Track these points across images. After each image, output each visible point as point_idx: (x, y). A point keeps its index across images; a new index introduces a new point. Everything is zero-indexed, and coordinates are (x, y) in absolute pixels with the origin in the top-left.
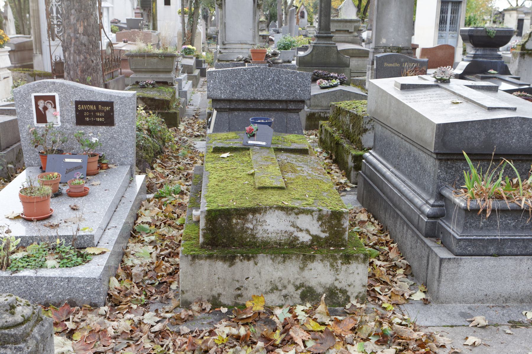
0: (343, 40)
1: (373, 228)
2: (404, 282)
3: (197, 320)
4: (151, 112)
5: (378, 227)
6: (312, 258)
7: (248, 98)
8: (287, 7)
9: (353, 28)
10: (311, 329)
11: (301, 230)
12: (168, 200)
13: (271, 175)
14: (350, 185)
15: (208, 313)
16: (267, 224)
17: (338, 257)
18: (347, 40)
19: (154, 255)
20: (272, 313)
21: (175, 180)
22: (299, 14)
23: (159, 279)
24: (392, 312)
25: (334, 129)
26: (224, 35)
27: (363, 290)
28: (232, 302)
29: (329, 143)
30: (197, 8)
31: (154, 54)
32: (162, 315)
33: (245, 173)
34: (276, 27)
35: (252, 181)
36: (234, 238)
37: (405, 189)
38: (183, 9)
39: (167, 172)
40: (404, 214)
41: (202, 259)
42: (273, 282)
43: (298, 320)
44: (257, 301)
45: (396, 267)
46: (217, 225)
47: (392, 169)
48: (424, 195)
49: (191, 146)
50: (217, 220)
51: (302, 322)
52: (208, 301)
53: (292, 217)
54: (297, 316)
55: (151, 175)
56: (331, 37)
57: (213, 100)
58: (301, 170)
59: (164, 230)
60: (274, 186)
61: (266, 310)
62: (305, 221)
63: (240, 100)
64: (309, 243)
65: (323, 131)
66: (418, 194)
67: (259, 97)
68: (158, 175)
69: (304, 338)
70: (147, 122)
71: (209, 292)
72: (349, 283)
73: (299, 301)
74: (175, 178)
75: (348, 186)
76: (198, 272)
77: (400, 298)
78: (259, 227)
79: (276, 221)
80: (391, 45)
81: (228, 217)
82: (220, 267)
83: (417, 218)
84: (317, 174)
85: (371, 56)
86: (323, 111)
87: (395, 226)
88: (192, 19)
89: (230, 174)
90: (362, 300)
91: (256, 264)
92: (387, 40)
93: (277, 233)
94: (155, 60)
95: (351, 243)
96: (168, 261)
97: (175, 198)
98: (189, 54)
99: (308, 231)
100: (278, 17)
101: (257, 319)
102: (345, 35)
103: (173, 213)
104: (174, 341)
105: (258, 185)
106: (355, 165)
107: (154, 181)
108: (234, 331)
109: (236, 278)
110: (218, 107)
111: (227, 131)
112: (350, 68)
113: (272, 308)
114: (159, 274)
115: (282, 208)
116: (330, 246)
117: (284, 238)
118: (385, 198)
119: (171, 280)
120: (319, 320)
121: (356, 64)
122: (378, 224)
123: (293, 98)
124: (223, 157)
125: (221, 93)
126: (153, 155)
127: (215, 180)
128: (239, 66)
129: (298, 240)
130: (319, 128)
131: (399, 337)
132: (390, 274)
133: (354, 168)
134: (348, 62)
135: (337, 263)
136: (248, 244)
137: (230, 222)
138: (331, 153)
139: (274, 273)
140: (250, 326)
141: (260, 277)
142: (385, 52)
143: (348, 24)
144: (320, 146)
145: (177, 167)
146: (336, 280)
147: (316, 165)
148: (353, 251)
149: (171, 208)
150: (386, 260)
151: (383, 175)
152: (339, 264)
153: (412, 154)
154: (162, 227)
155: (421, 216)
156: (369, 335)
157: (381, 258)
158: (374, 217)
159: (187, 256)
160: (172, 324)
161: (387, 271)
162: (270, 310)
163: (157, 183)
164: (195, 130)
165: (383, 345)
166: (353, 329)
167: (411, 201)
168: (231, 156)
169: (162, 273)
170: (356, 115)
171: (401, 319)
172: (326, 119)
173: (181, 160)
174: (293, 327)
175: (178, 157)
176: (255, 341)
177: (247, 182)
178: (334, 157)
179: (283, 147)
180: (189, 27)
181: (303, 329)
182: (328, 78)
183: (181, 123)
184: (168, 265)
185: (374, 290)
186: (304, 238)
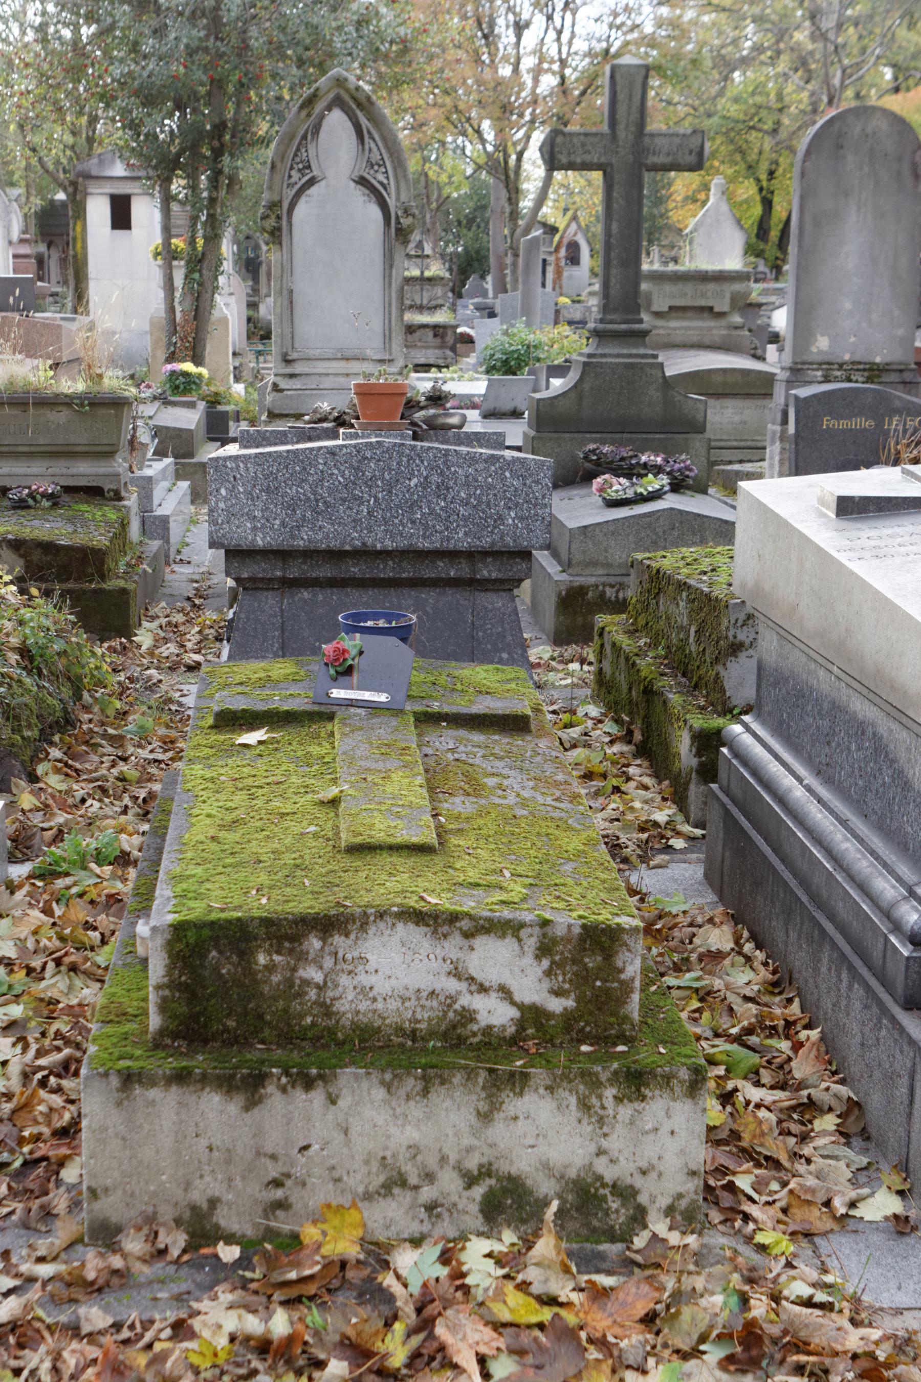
0: (695, 339)
2: (836, 1158)
3: (140, 1286)
4: (34, 591)
5: (765, 974)
6: (518, 1082)
7: (344, 544)
8: (518, 231)
9: (727, 300)
10: (506, 1316)
11: (483, 989)
12: (75, 884)
13: (395, 803)
14: (687, 829)
15: (177, 1262)
16: (371, 967)
17: (604, 1077)
18: (706, 341)
19: (14, 1069)
20: (387, 1263)
21: (106, 817)
22: (563, 252)
23: (26, 1149)
24: (783, 1261)
25: (642, 642)
26: (287, 331)
27: (691, 1187)
28: (256, 1225)
29: (625, 688)
30: (213, 239)
31: (57, 396)
32: (24, 1268)
33: (309, 797)
34: (484, 294)
35: (329, 825)
36: (260, 1016)
37: (845, 845)
38: (167, 243)
39: (80, 789)
40: (842, 929)
41: (154, 1084)
42: (389, 1160)
43: (466, 1290)
44: (336, 1222)
45: (811, 1108)
46: (207, 973)
47: (809, 779)
48: (904, 870)
49: (170, 700)
50: (203, 957)
51: (480, 1295)
52: (178, 1222)
53: (453, 947)
54: (463, 1275)
55: (27, 800)
56: (644, 334)
57: (228, 552)
58: (500, 787)
59: (54, 985)
61: (369, 1253)
62: (494, 959)
63: (317, 552)
64: (511, 1030)
65: (608, 648)
66: (885, 865)
67: (381, 540)
68: (50, 802)
69: (483, 1349)
70: (21, 623)
71: (178, 1194)
72: (644, 1164)
73: (478, 1222)
74: (108, 811)
75: (679, 834)
76: (140, 1126)
77: (818, 1213)
78: (344, 980)
79: (398, 959)
80: (847, 357)
81: (243, 946)
83: (880, 946)
84: (549, 801)
85: (779, 392)
86: (611, 580)
87: (816, 970)
88: (196, 276)
89: (259, 803)
90: (685, 1217)
91: (333, 1102)
92: (833, 339)
93: (404, 1000)
94: (61, 416)
95: (653, 1029)
96: (58, 1090)
97: (104, 879)
98: (186, 391)
99: (505, 992)
100: (492, 260)
101: (336, 1283)
102: (700, 324)
103: (88, 926)
104: (57, 1357)
105: (346, 838)
106: (701, 764)
107: (37, 819)
108: (253, 1325)
109: (269, 1148)
110: (245, 575)
111: (276, 655)
112: (709, 434)
113: (388, 1248)
114: (26, 1134)
115: (418, 917)
116: (581, 1042)
117: (426, 1015)
118: (787, 875)
119: (64, 1151)
120: (536, 1289)
121: (737, 419)
122: (765, 964)
123: (493, 543)
124: (245, 746)
125: (254, 529)
127: (208, 821)
128: (318, 438)
129: (472, 1020)
130: (596, 637)
131: (801, 1346)
132: (789, 1133)
133: (698, 772)
134: (700, 417)
135: (600, 1097)
136: (309, 1035)
137: (249, 963)
138: (631, 723)
139: (393, 1130)
140: (309, 1308)
141: (348, 1143)
142: (827, 380)
143: (711, 286)
144: (596, 698)
145: (115, 771)
146: (600, 1152)
147: (549, 768)
148: (655, 1058)
149: (80, 912)
150: (781, 1086)
151: (782, 800)
152: (609, 1102)
153: (869, 733)
154: (48, 974)
155: (892, 938)
156: (703, 1339)
157: (766, 1077)
158: (753, 937)
159: (106, 1075)
160: (56, 1301)
161: (780, 1122)
162: (378, 1255)
163: (45, 825)
164: (189, 645)
165: (744, 1372)
166: (649, 1319)
167: (863, 888)
168: (273, 741)
169: (35, 1130)
170: (708, 596)
171: (814, 1285)
172: (619, 607)
173: (130, 750)
174: (449, 1312)
175: (121, 738)
176: (322, 1356)
177: (312, 829)
178: (638, 737)
179: (447, 709)
180: (188, 303)
181: (482, 1317)
182: (631, 471)
183: (145, 624)
184: (57, 1100)
185: (731, 1187)
186: (495, 1014)
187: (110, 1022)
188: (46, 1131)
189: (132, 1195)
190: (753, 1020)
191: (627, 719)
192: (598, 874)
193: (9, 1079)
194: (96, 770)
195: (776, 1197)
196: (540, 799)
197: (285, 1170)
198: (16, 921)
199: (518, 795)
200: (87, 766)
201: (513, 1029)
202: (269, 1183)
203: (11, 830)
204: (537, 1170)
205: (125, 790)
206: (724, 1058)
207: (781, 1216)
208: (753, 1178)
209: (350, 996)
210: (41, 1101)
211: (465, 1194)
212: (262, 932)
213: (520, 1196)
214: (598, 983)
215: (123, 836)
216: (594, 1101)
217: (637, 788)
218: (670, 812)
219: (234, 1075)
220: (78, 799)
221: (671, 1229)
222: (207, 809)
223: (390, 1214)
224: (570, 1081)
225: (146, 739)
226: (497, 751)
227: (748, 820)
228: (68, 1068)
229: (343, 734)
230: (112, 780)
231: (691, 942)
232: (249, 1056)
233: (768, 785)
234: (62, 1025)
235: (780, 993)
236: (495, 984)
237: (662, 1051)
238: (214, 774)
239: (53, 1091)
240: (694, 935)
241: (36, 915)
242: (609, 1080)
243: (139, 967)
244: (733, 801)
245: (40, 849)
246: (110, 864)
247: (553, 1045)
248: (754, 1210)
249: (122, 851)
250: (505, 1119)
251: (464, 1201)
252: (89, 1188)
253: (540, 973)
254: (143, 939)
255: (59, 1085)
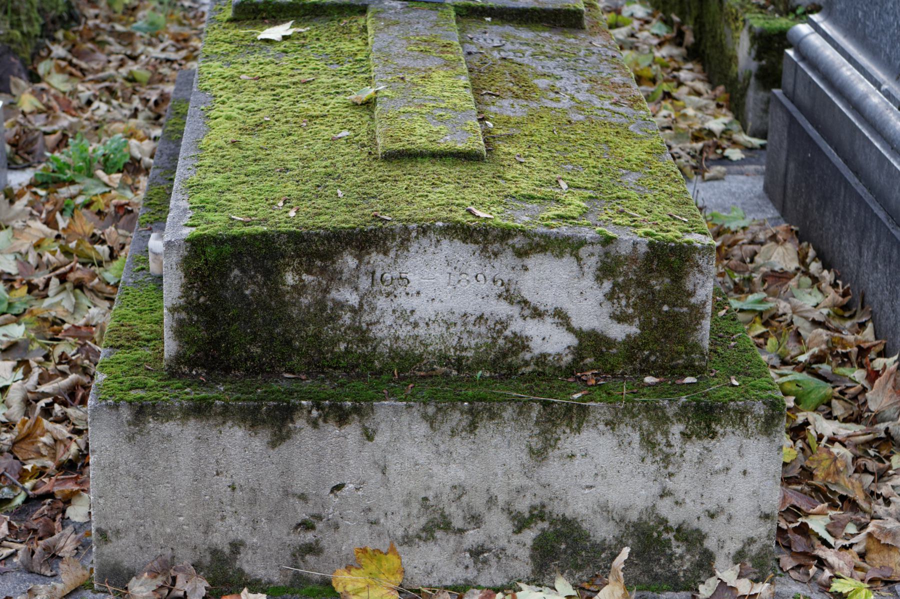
1: (818, 298)
5: (833, 296)
6: (576, 416)
11: (537, 314)
12: (80, 193)
14: (743, 138)
16: (413, 287)
17: (670, 411)
19: (15, 396)
21: (114, 120)
23: (28, 485)
27: (763, 531)
33: (341, 98)
35: (364, 129)
36: (288, 343)
39: (85, 91)
41: (169, 417)
42: (432, 502)
44: (372, 568)
46: (228, 295)
50: (224, 275)
53: (503, 266)
55: (28, 102)
58: (552, 89)
59: (57, 302)
60: (442, 147)
64: (568, 359)
68: (54, 103)
71: (198, 537)
72: (713, 508)
75: (735, 144)
78: (382, 303)
79: (443, 280)
82: (238, 447)
84: (607, 104)
89: (285, 104)
91: (370, 438)
93: (449, 325)
95: (723, 359)
96: (64, 419)
97: (111, 187)
99: (562, 317)
103: (96, 240)
105: (383, 144)
107: (39, 123)
114: (28, 467)
116: (645, 372)
117: (473, 342)
118: (861, 189)
119: (71, 487)
122: (835, 285)
124: (268, 41)
126: (37, 29)
127: (228, 124)
129: (525, 348)
132: (866, 471)
133: (757, 77)
135: (666, 433)
136: (343, 363)
138: (682, 23)
139: (436, 469)
141: (386, 483)
145: (124, 71)
146: (665, 494)
147: (606, 69)
148: (728, 391)
149: (86, 224)
150: (855, 419)
151: (857, 107)
154: (52, 290)
157: (839, 409)
158: (820, 256)
159: (116, 406)
161: (855, 458)
163: (48, 129)
169: (38, 463)
177: (345, 133)
178: (689, 38)
184: (62, 431)
185: (804, 530)
186: (550, 341)
187: (121, 346)
188: (50, 464)
189: (146, 537)
190: (824, 347)
191: (676, 19)
192: (664, 186)
193: (9, 407)
194: (103, 70)
195: (853, 541)
196: (597, 103)
197: (315, 511)
198: (17, 233)
199: (573, 98)
200: (94, 65)
201: (569, 358)
202: (299, 525)
203: (10, 134)
204: (595, 512)
205: (135, 92)
206: (793, 388)
207: (858, 561)
208: (827, 520)
209: (389, 320)
210: (45, 432)
211: (516, 538)
212: (290, 249)
213: (575, 541)
214: (665, 308)
215: (133, 142)
216: (659, 437)
217: (690, 94)
218: (726, 120)
219: (260, 407)
220: (84, 101)
221: (740, 577)
222: (226, 111)
223: (432, 560)
224: (634, 416)
225: (157, 36)
226: (547, 49)
227: (817, 128)
228: (74, 395)
229: (378, 30)
230: (120, 80)
231: (752, 261)
232: (275, 387)
233: (842, 90)
234: (66, 348)
235: (851, 317)
236: (550, 309)
237: (735, 383)
238: (234, 72)
239: (58, 421)
240: (756, 253)
241: (38, 227)
242: (676, 415)
243: (152, 286)
244: (799, 107)
245: (43, 155)
246: (119, 171)
247: (614, 376)
248: (830, 556)
249: (132, 158)
250: (561, 457)
251: (514, 545)
252: (98, 530)
253: (601, 296)
254: (156, 254)
255: (64, 414)
